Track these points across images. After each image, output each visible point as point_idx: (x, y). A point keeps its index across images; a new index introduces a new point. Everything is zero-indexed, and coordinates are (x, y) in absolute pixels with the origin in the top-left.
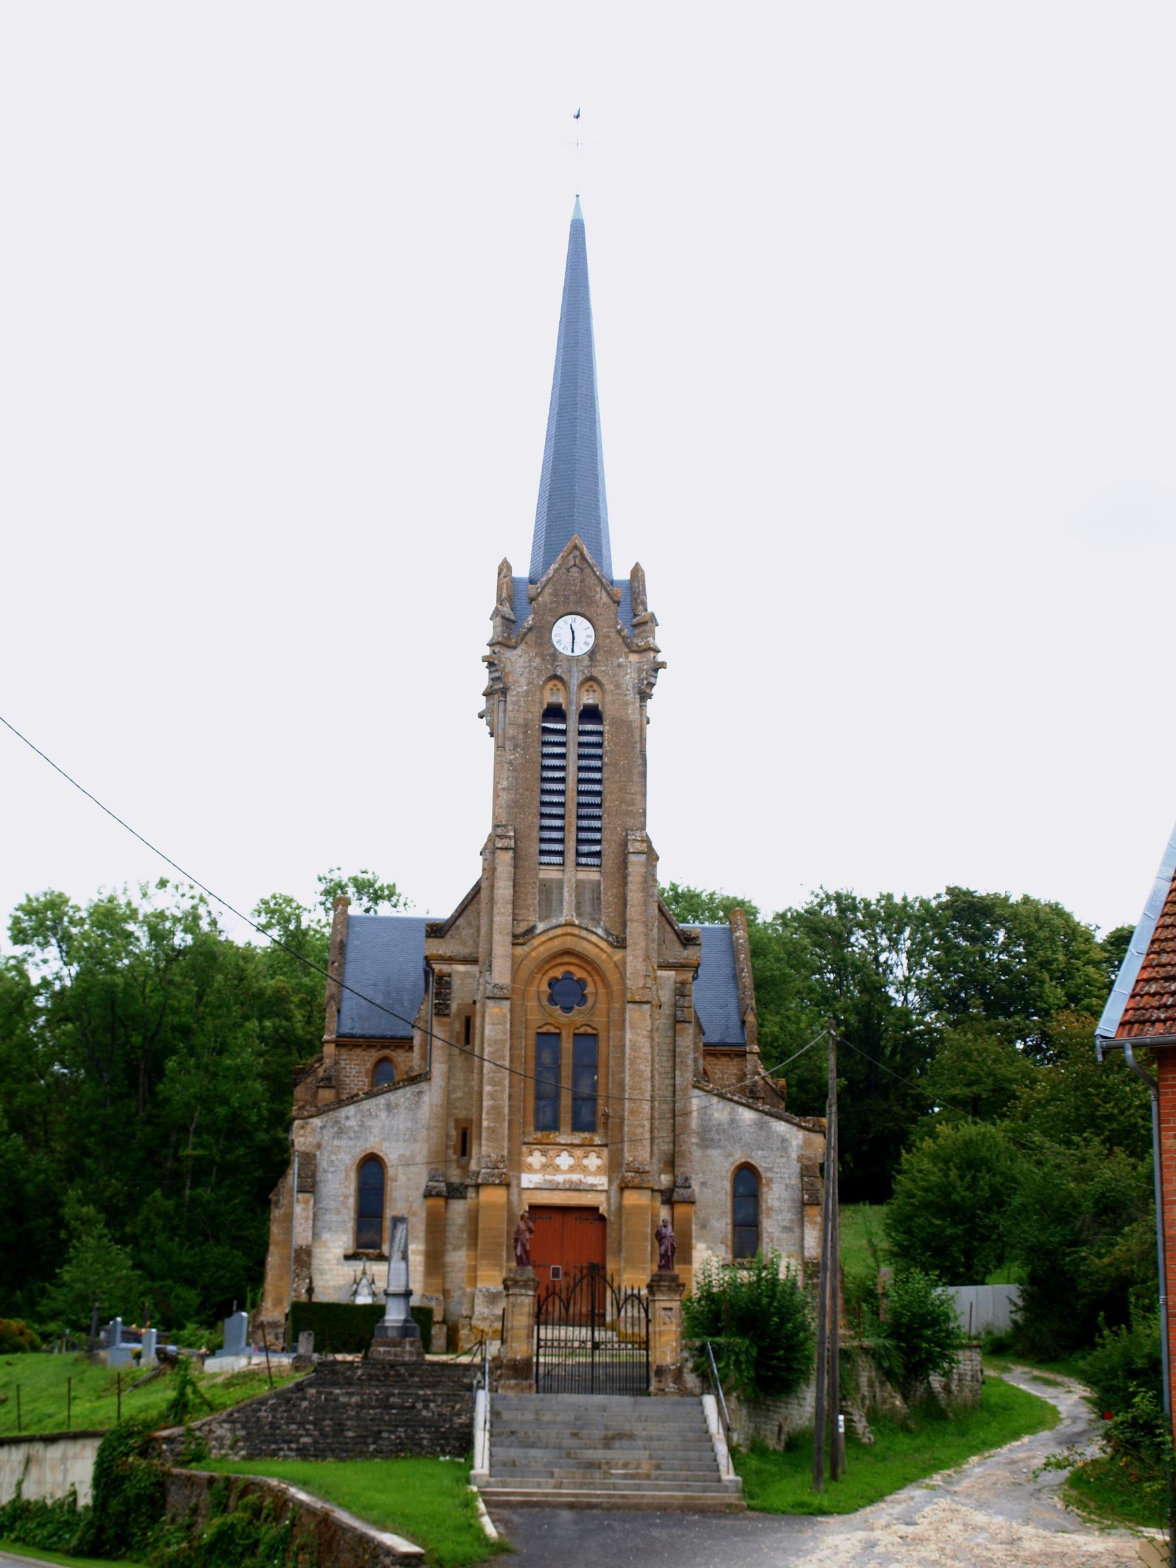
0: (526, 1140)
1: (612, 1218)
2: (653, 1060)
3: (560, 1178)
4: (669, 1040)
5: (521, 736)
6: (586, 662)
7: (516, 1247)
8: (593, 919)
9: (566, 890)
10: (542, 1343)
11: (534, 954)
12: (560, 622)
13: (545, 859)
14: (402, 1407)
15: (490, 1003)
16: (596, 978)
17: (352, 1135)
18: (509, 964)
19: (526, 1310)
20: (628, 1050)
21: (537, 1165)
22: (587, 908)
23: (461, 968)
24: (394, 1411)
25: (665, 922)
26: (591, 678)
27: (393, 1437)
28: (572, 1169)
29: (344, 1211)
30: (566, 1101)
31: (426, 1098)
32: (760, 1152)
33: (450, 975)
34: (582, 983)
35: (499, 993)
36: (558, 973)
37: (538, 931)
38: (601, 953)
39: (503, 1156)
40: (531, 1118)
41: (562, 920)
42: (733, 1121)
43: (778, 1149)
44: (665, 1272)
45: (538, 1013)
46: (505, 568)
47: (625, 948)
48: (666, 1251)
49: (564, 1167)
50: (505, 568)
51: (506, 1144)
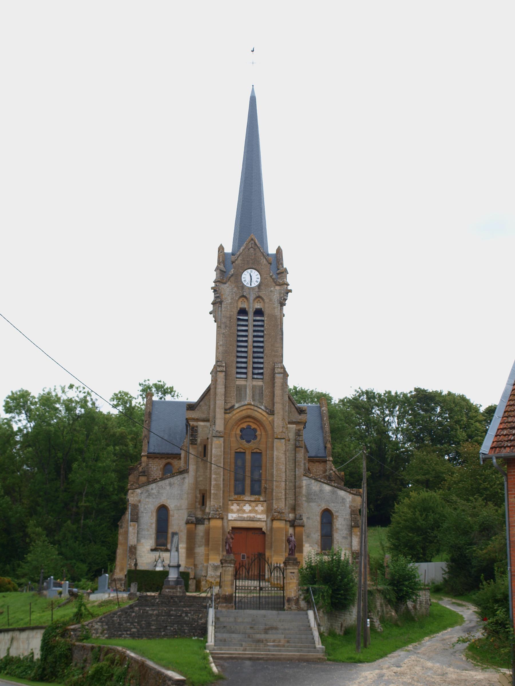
0: (230, 499)
1: (268, 533)
2: (286, 464)
3: (245, 515)
4: (293, 455)
5: (228, 322)
6: (257, 290)
7: (226, 546)
8: (260, 402)
9: (248, 389)
10: (237, 588)
11: (234, 417)
12: (245, 272)
17: (154, 496)
18: (223, 422)
21: (235, 510)
22: (257, 397)
23: (202, 424)
24: (173, 617)
25: (291, 404)
26: (259, 297)
27: (172, 629)
28: (250, 512)
30: (248, 482)
31: (186, 481)
33: (197, 427)
34: (255, 430)
35: (218, 435)
36: (244, 425)
37: (236, 407)
38: (263, 417)
39: (220, 506)
40: (232, 489)
41: (246, 403)
42: (321, 490)
43: (341, 503)
44: (291, 557)
45: (236, 443)
46: (221, 249)
47: (274, 415)
48: (292, 547)
49: (247, 511)
50: (221, 249)
51: (221, 500)
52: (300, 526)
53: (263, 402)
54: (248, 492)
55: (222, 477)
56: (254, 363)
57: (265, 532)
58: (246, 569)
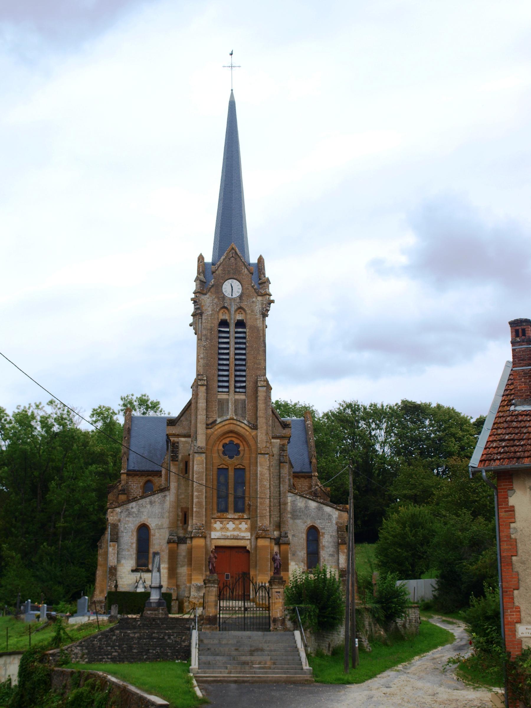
0: (213, 517)
3: (229, 534)
5: (209, 334)
6: (238, 301)
8: (242, 417)
11: (216, 433)
12: (226, 283)
13: (220, 390)
14: (158, 638)
15: (196, 455)
16: (244, 443)
18: (205, 437)
19: (214, 593)
21: (218, 528)
22: (240, 412)
23: (183, 439)
24: (155, 640)
25: (275, 418)
27: (154, 652)
28: (234, 530)
29: (131, 550)
30: (231, 499)
31: (168, 498)
32: (319, 521)
33: (178, 443)
34: (238, 446)
35: (200, 450)
36: (227, 441)
37: (218, 422)
38: (246, 432)
39: (203, 524)
40: (215, 506)
41: (228, 417)
42: (306, 507)
43: (327, 519)
45: (218, 460)
46: (201, 258)
48: (277, 566)
49: (231, 529)
50: (201, 258)
51: (204, 519)
53: (246, 417)
56: (236, 376)
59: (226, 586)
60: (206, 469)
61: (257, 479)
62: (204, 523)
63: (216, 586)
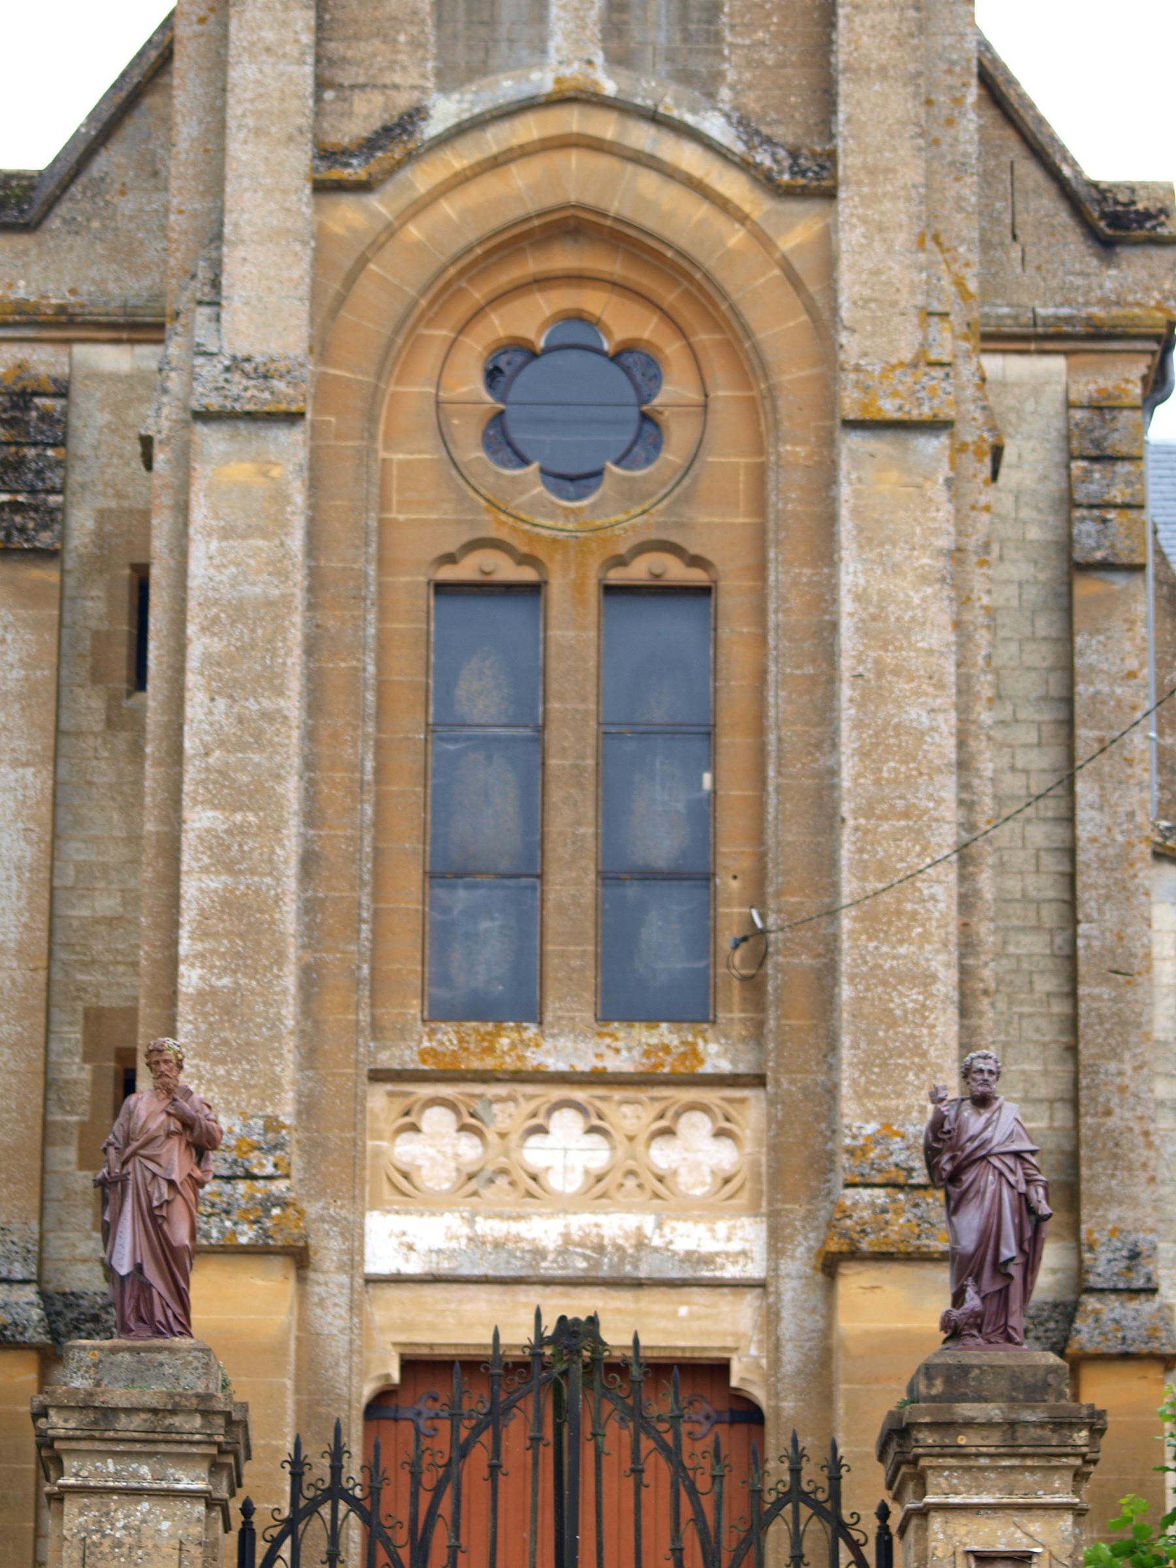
0: (387, 1059)
1: (788, 1405)
2: (965, 688)
3: (544, 1231)
4: (1041, 656)
7: (108, 1232)
8: (685, 77)
11: (414, 232)
15: (212, 441)
16: (704, 338)
18: (300, 271)
20: (848, 640)
23: (114, 357)
25: (1015, 149)
28: (599, 1189)
30: (571, 885)
33: (62, 390)
34: (636, 364)
35: (247, 393)
36: (530, 319)
37: (432, 129)
38: (720, 223)
39: (272, 1125)
40: (406, 959)
41: (543, 81)
44: (977, 1354)
45: (435, 495)
47: (830, 195)
48: (990, 1236)
49: (565, 1180)
51: (287, 1068)
52: (1126, 1357)
53: (717, 77)
54: (570, 992)
55: (293, 828)
57: (760, 1395)
58: (354, 1503)
59: (335, 1492)
60: (316, 582)
61: (831, 680)
62: (287, 1112)
63: (191, 1479)
